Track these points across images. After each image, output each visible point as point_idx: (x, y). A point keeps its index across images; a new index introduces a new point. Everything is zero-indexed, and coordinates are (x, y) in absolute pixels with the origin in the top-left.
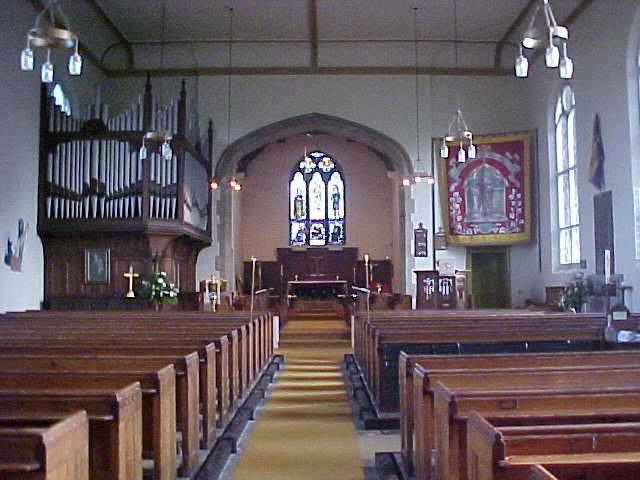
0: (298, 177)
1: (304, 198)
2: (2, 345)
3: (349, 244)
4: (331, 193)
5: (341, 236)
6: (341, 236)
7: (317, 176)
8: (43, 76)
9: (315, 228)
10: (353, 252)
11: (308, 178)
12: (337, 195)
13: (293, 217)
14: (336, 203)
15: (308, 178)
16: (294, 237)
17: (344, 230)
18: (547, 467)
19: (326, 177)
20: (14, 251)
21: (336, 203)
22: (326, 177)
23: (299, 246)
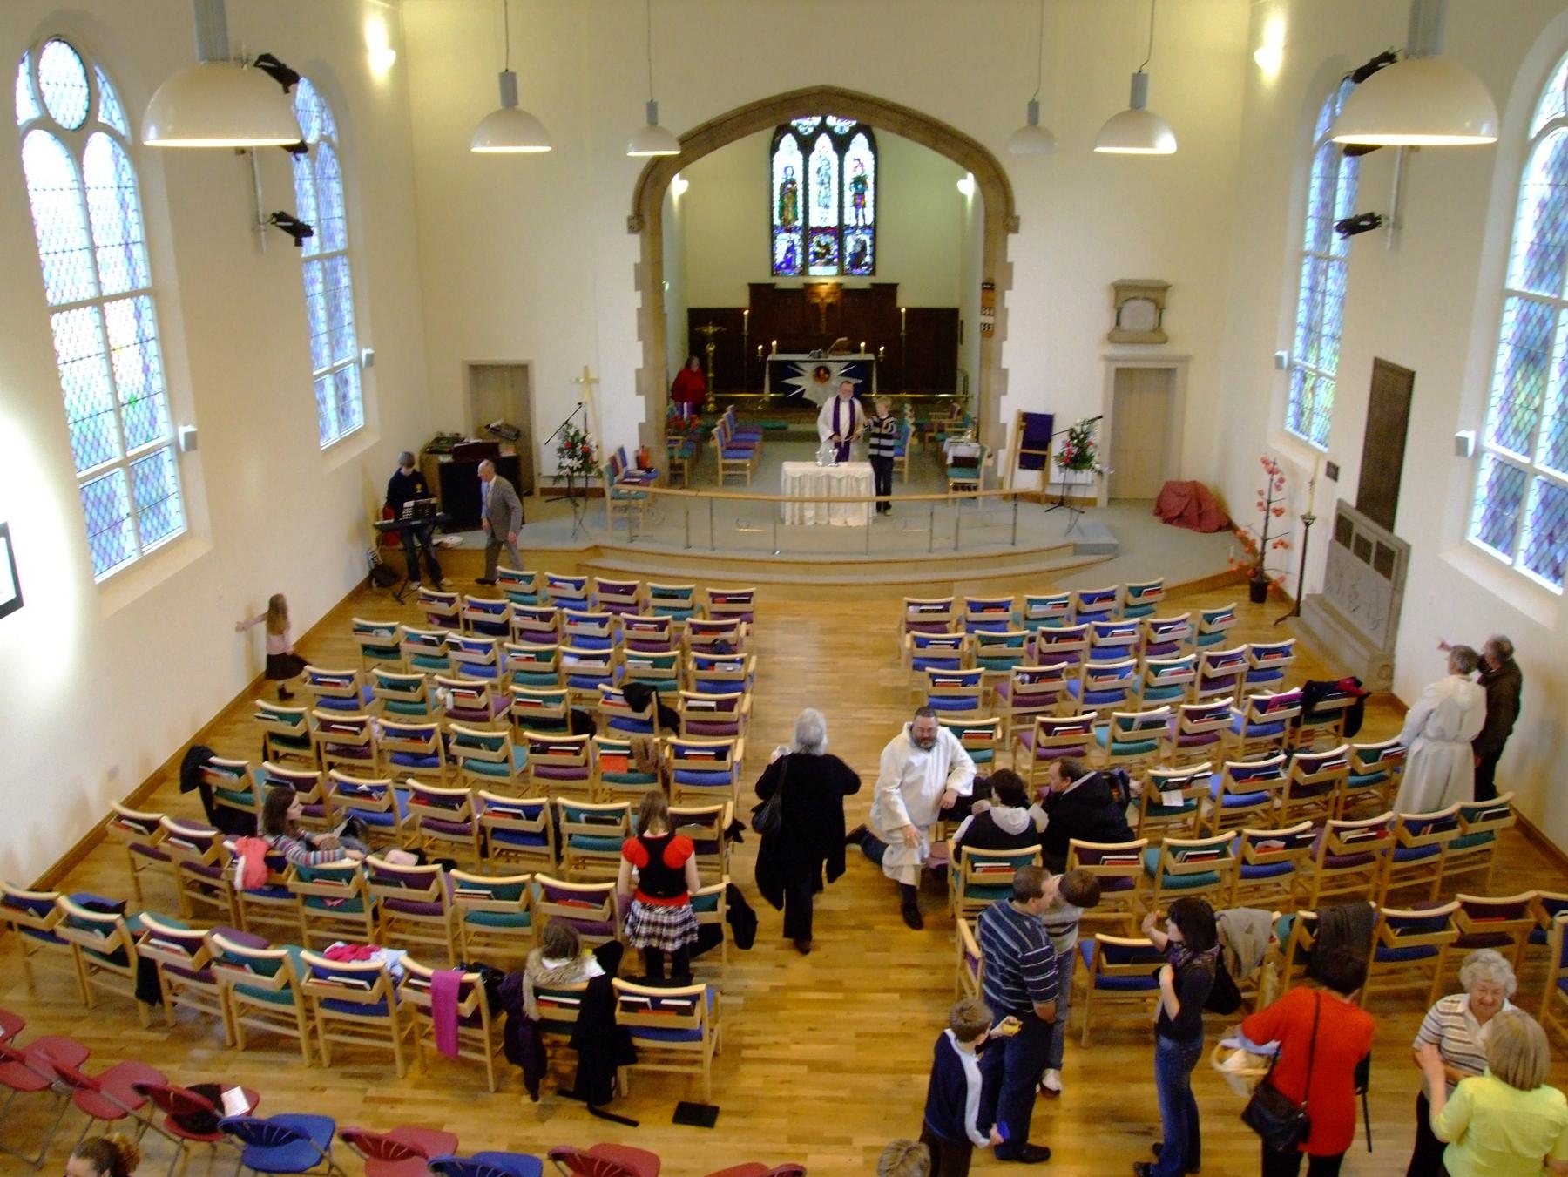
0: (788, 142)
1: (800, 186)
2: (25, 996)
3: (882, 277)
4: (849, 178)
5: (868, 259)
6: (868, 259)
7: (824, 142)
8: (148, 314)
9: (819, 245)
10: (890, 290)
11: (806, 145)
12: (859, 181)
13: (777, 222)
14: (859, 195)
15: (806, 145)
16: (780, 258)
17: (874, 246)
18: (975, 973)
19: (842, 144)
20: (627, 743)
21: (859, 195)
22: (842, 144)
23: (788, 281)
